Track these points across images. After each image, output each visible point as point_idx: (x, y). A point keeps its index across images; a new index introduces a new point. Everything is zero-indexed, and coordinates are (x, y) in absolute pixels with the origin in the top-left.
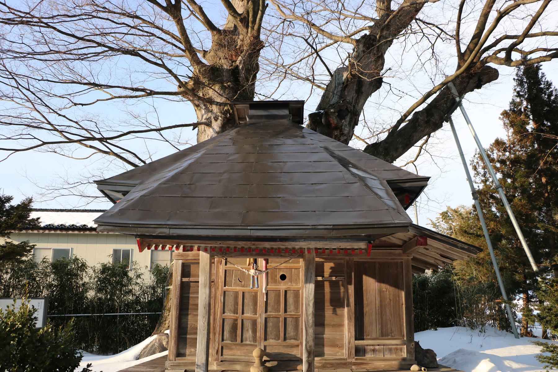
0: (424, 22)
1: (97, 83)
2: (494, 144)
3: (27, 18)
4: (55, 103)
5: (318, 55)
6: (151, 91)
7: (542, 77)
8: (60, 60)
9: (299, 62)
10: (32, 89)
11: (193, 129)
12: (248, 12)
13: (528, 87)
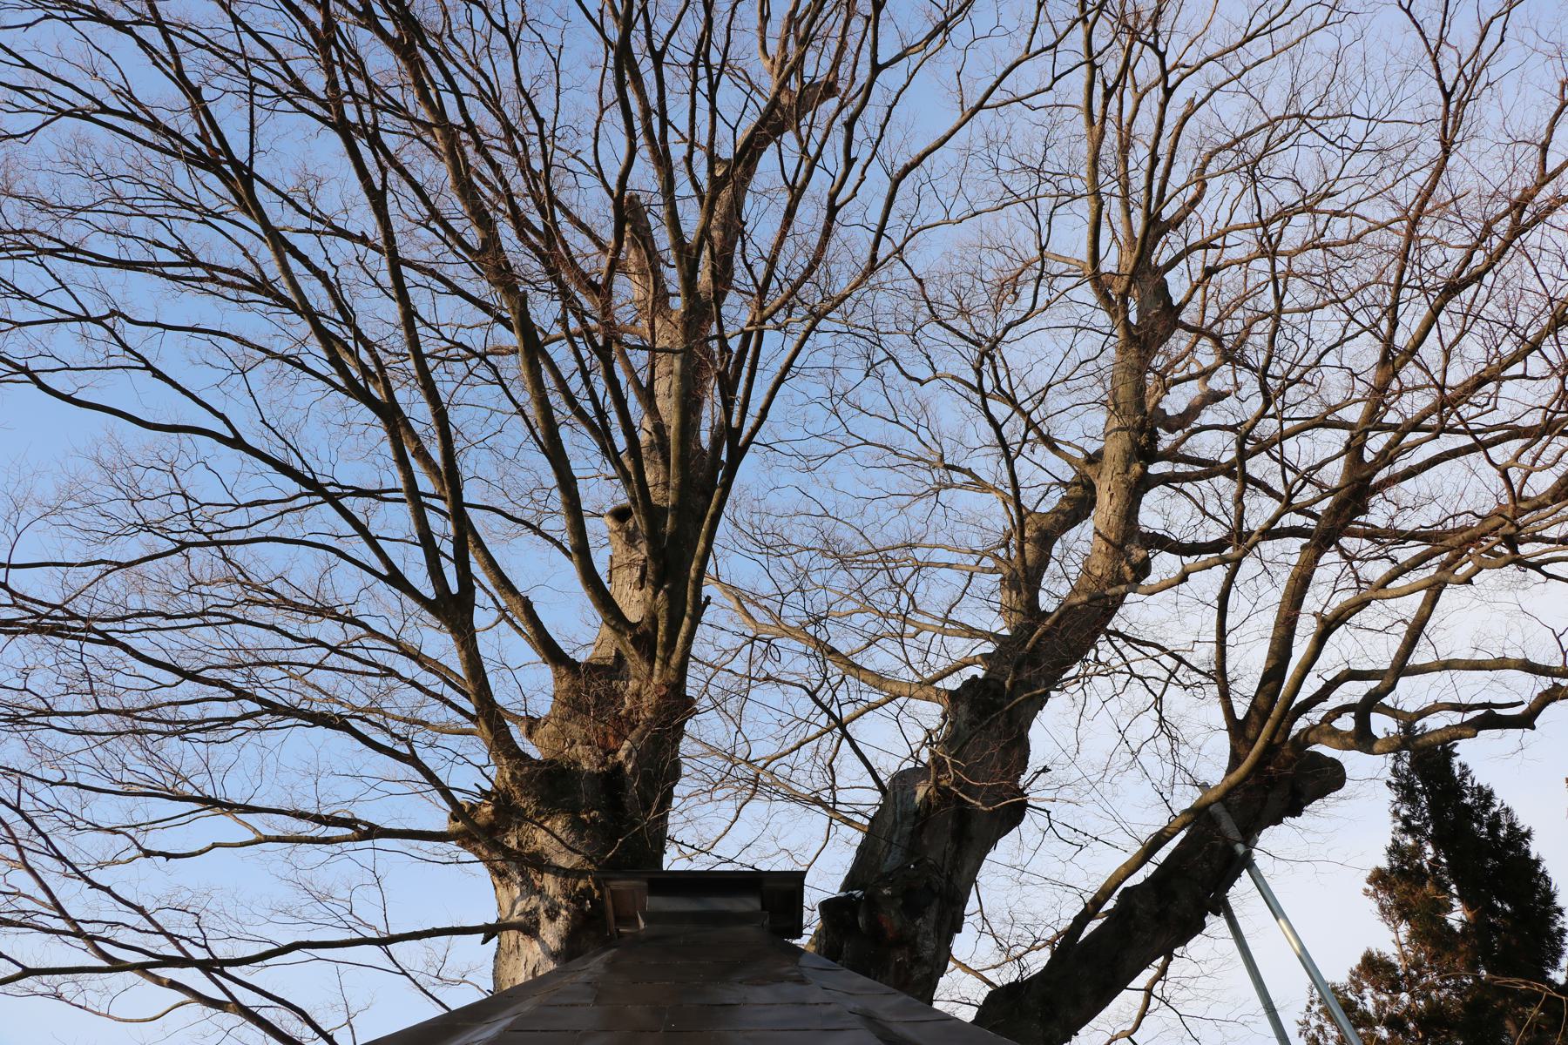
0: (1127, 639)
1: (221, 797)
2: (1359, 967)
3: (56, 618)
4: (85, 847)
5: (845, 735)
6: (372, 826)
7: (1464, 776)
8: (119, 734)
9: (792, 750)
10: (27, 804)
11: (484, 942)
12: (654, 620)
13: (1431, 805)
